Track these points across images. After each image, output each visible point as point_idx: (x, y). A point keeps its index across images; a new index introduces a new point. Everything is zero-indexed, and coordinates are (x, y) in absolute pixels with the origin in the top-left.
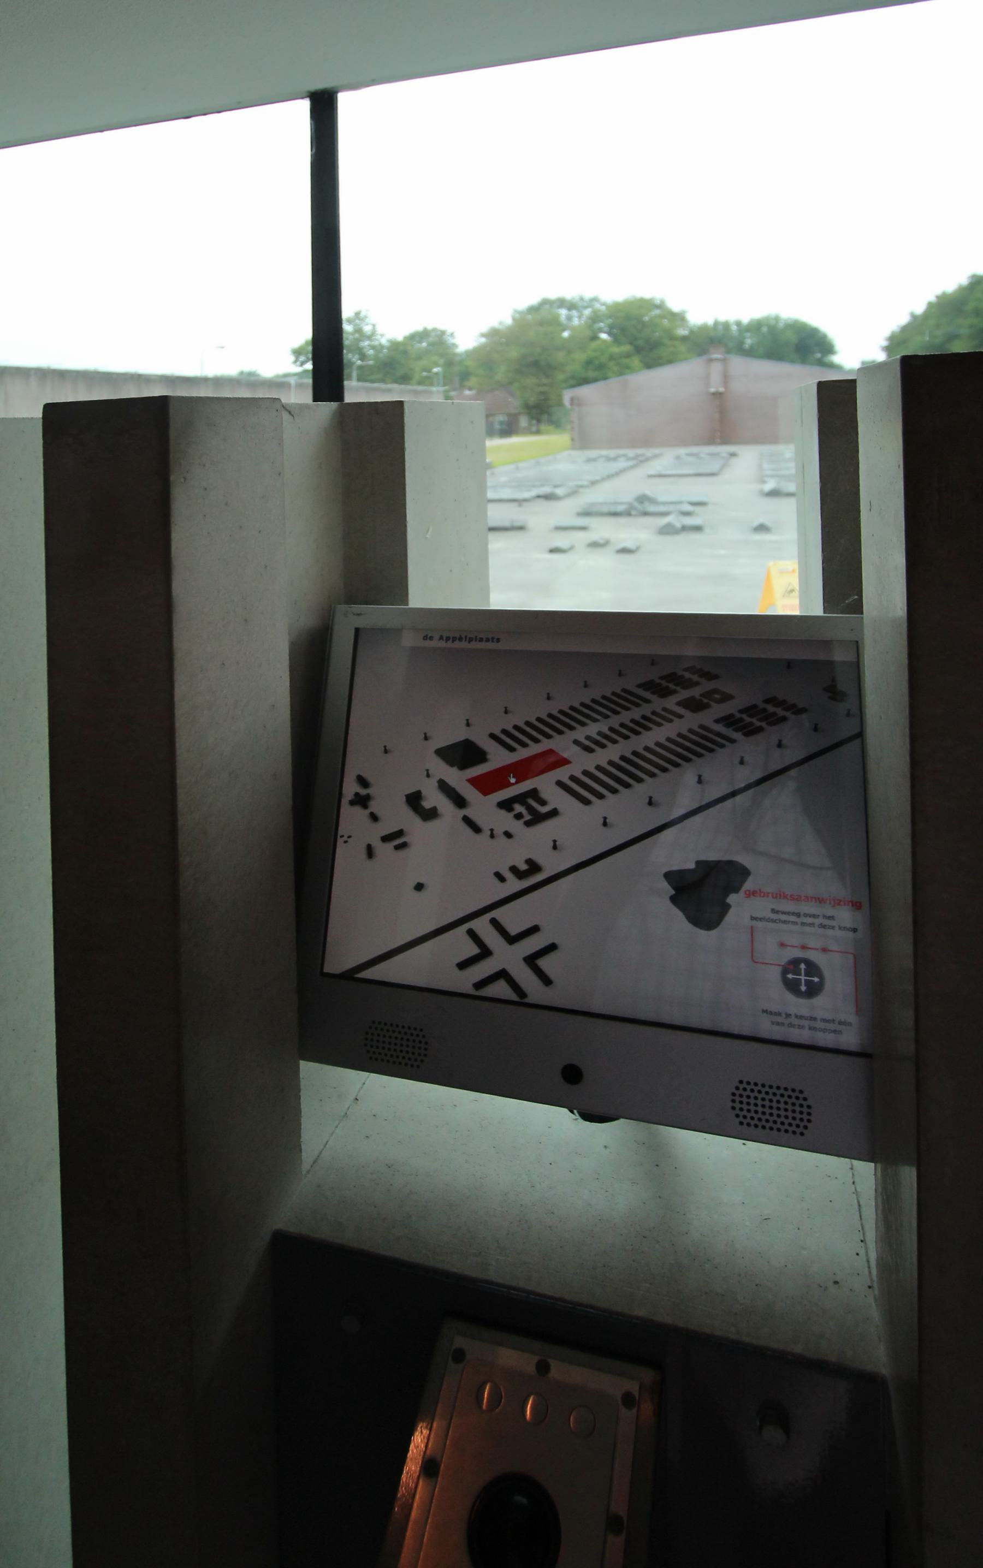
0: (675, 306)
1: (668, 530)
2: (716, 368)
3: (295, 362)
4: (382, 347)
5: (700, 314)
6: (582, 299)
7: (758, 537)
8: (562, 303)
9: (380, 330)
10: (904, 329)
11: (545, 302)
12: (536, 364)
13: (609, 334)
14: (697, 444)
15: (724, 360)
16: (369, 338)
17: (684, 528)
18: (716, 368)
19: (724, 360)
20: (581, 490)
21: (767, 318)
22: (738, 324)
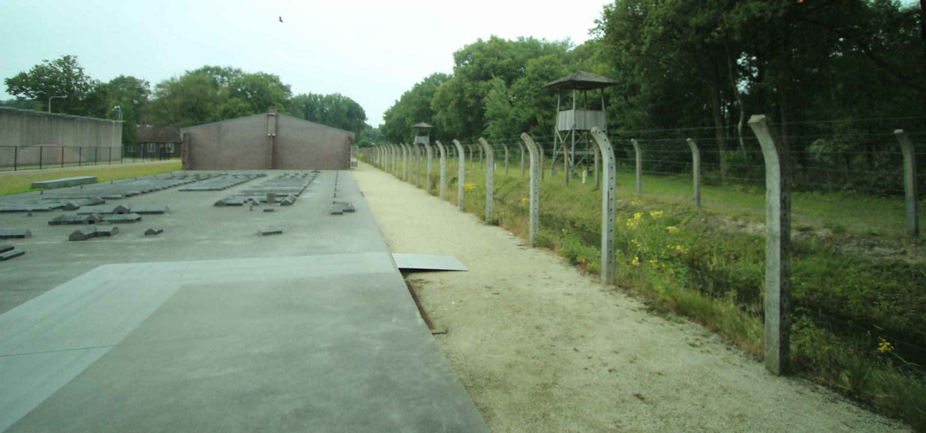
0: (284, 81)
1: (76, 237)
2: (272, 121)
3: (9, 90)
4: (87, 87)
5: (299, 89)
6: (231, 70)
7: (148, 240)
8: (217, 70)
9: (86, 73)
10: (393, 109)
11: (207, 69)
12: (193, 109)
13: (894, 136)
14: (262, 169)
15: (276, 116)
16: (76, 78)
17: (96, 235)
18: (272, 121)
19: (276, 116)
20: (107, 201)
21: (335, 95)
22: (321, 97)
